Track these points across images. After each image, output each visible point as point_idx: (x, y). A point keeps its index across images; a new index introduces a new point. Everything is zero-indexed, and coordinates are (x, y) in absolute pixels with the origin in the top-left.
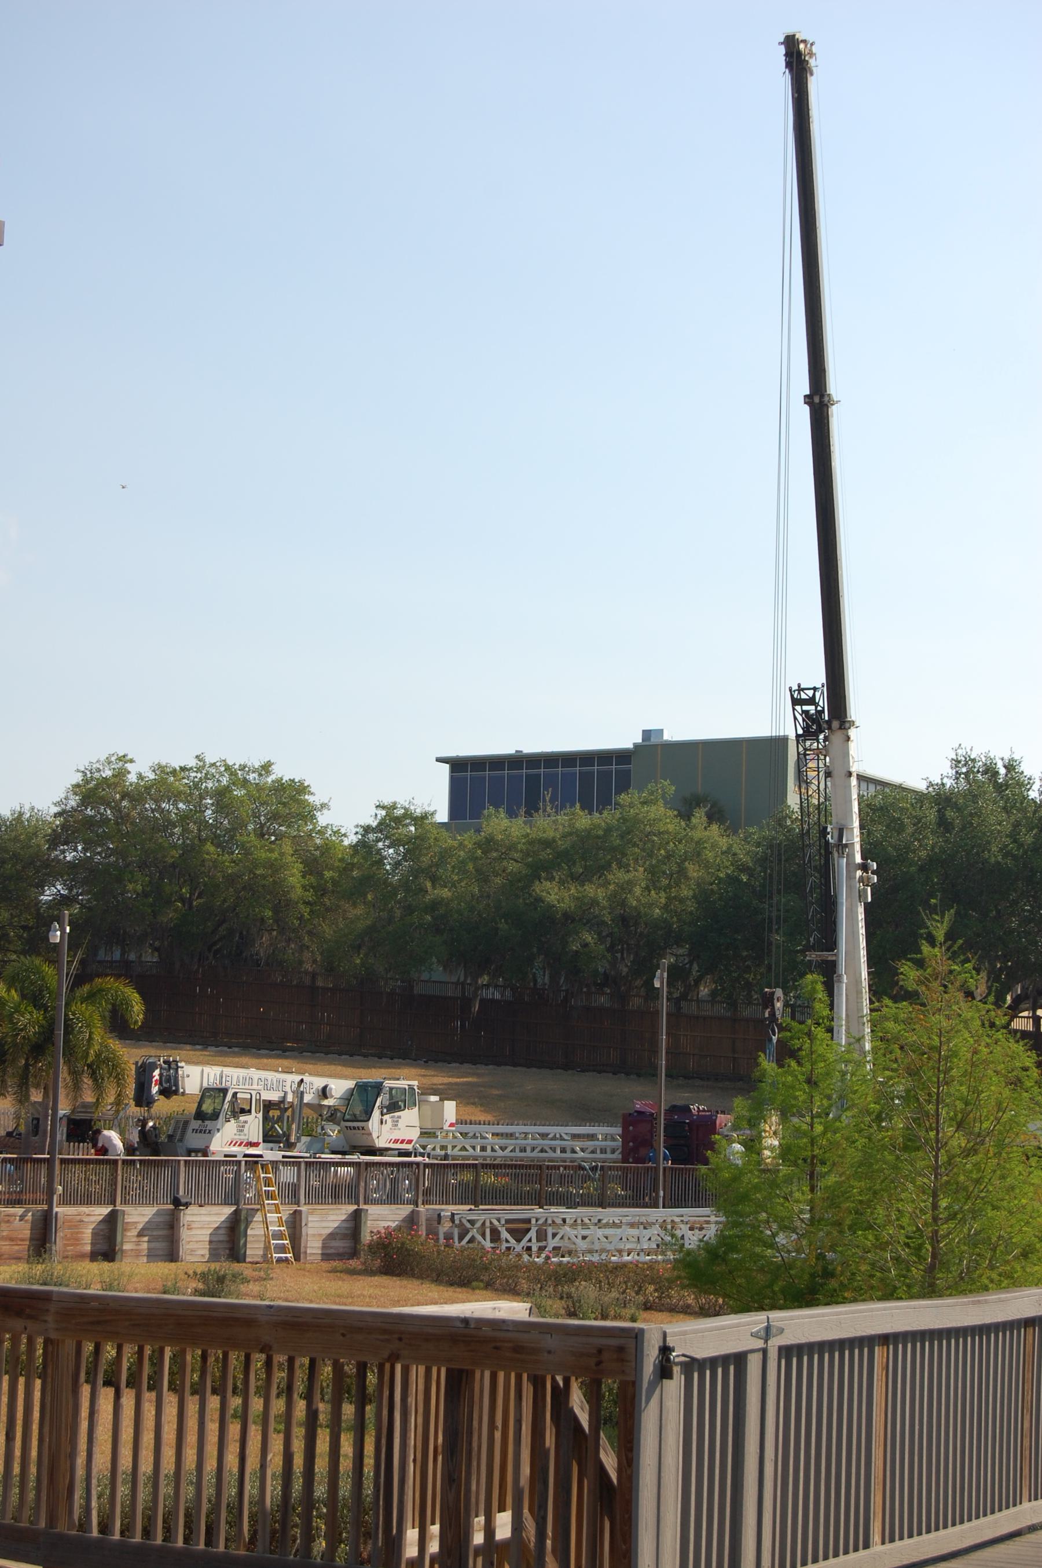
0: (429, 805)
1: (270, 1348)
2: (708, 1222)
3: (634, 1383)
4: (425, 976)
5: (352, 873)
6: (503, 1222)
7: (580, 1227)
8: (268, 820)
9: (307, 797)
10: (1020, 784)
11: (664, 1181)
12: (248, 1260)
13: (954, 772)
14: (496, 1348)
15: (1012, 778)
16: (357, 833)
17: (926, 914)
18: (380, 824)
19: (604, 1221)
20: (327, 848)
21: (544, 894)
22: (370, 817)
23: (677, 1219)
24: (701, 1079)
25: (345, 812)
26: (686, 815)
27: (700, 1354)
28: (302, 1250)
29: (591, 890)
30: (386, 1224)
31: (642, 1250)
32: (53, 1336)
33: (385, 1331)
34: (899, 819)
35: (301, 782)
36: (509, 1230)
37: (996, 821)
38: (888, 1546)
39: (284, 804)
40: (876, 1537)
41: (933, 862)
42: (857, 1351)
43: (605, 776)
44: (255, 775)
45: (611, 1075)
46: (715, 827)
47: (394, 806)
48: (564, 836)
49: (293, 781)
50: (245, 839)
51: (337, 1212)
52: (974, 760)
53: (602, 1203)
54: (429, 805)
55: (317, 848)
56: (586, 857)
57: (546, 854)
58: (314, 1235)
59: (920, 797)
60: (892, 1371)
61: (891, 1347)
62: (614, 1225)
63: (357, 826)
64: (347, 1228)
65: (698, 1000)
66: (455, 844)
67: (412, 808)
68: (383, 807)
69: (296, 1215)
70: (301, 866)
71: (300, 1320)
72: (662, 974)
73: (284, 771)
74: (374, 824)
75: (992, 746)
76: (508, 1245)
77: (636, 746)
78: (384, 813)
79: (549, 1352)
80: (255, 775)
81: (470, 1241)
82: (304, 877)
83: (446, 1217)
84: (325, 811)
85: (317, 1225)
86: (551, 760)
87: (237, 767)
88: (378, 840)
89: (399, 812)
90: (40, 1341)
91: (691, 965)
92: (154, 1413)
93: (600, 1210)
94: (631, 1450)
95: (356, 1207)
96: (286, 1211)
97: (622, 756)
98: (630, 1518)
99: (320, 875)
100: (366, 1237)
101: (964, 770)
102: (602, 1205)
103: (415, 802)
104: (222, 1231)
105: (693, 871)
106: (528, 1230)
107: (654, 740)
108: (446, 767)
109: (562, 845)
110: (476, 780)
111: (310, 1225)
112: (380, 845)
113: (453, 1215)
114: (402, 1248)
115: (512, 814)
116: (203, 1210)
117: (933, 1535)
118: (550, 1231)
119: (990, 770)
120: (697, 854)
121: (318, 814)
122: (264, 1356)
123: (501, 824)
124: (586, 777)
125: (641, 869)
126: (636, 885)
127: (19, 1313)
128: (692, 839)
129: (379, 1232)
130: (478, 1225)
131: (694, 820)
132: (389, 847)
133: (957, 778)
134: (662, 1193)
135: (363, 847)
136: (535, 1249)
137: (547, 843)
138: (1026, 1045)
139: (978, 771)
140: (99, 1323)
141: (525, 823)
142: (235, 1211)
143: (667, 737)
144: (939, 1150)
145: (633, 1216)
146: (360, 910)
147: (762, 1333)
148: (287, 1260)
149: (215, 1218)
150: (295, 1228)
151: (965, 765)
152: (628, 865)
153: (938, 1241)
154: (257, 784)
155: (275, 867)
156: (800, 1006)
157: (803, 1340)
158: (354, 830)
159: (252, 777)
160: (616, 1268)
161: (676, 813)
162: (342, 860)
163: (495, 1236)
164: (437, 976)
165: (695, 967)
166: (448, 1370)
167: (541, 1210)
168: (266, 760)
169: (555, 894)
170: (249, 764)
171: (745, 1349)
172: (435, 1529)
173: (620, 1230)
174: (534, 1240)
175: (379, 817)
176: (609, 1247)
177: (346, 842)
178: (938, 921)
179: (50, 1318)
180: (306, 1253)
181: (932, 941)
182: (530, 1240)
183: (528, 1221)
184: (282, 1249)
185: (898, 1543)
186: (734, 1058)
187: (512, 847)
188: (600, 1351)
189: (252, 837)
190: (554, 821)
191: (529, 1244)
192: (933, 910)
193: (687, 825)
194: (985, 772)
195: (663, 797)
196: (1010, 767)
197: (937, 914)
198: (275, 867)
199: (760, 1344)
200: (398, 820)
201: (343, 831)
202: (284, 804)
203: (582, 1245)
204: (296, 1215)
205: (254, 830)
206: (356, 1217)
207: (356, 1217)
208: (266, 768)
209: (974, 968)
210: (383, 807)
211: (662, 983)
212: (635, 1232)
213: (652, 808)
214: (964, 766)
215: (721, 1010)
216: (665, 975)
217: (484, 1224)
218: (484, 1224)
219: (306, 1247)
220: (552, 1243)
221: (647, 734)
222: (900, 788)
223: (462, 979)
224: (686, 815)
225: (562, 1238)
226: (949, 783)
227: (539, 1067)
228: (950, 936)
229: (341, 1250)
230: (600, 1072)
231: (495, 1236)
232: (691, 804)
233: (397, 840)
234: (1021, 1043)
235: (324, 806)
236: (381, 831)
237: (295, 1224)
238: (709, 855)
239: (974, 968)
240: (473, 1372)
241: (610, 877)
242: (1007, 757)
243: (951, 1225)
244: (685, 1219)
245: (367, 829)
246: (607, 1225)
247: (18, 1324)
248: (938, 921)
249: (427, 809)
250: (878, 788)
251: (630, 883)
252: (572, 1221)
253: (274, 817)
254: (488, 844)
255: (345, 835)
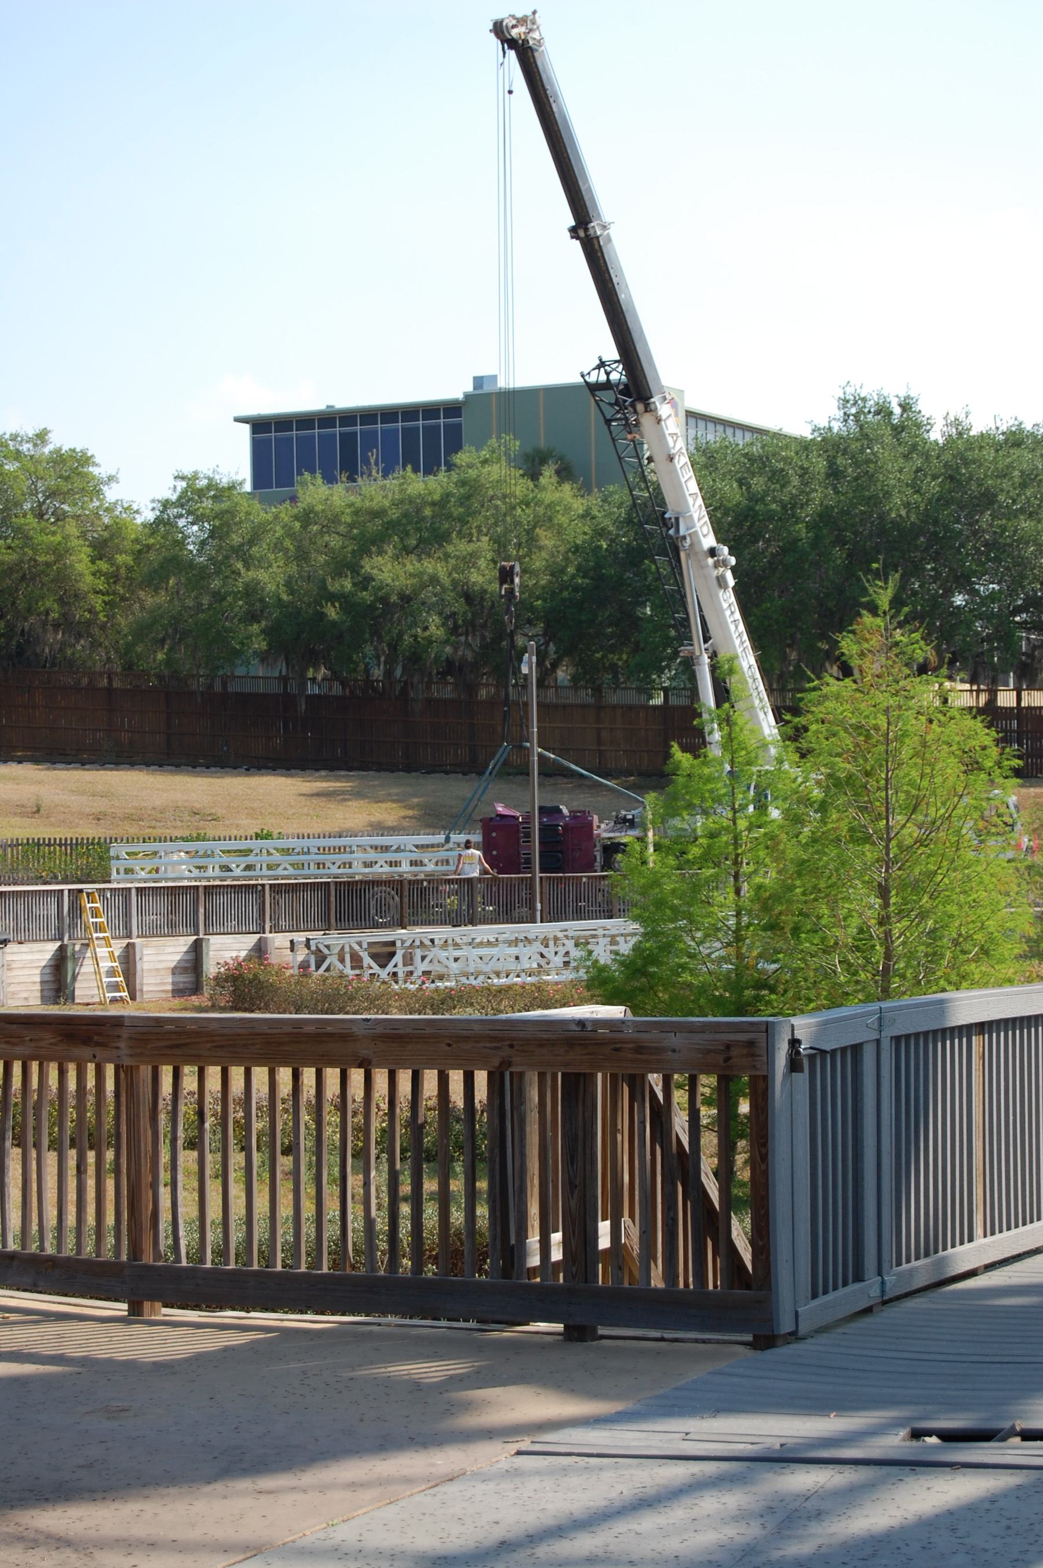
0: (237, 473)
1: (370, 1062)
2: (594, 936)
3: (765, 1078)
4: (240, 671)
5: (153, 556)
6: (365, 946)
7: (451, 948)
8: (47, 498)
9: (91, 469)
10: (919, 426)
11: (541, 893)
12: (77, 1001)
13: (842, 413)
14: (616, 1049)
15: (908, 419)
16: (153, 509)
17: (868, 581)
18: (180, 498)
19: (478, 940)
20: (116, 530)
21: (375, 571)
22: (168, 489)
23: (560, 935)
24: (564, 776)
25: (138, 484)
26: (534, 475)
27: (828, 1047)
28: (138, 987)
29: (431, 566)
30: (234, 954)
31: (523, 971)
32: (127, 1062)
33: (494, 1039)
34: (782, 470)
35: (83, 453)
36: (373, 956)
37: (894, 472)
38: (990, 1239)
39: (67, 479)
40: (979, 1230)
41: (825, 517)
42: (957, 1041)
43: (432, 432)
44: (30, 446)
45: (460, 776)
46: (567, 487)
47: (195, 477)
48: (395, 504)
49: (74, 450)
50: (22, 521)
51: (175, 943)
52: (864, 400)
53: (472, 921)
54: (237, 473)
55: (107, 527)
56: (422, 530)
57: (375, 527)
58: (150, 970)
59: (805, 446)
60: (988, 1060)
61: (986, 1036)
62: (489, 943)
63: (153, 501)
64: (186, 961)
65: (557, 687)
66: (269, 517)
67: (217, 477)
68: (183, 478)
69: (130, 949)
70: (89, 549)
71: (400, 1032)
72: (530, 658)
73: (62, 440)
74: (174, 497)
75: (884, 384)
76: (371, 971)
77: (467, 396)
78: (184, 484)
79: (674, 1051)
80: (30, 446)
81: (328, 970)
82: (93, 562)
83: (300, 943)
84: (113, 485)
85: (152, 958)
86: (369, 416)
87: (7, 436)
88: (181, 516)
89: (203, 483)
90: (110, 1070)
91: (547, 647)
92: (20, 1171)
93: (470, 927)
94: (765, 1145)
95: (195, 937)
96: (118, 946)
97: (452, 409)
98: (767, 1213)
99: (111, 560)
100: (211, 969)
101: (853, 411)
102: (472, 922)
103: (220, 470)
104: (47, 971)
105: (546, 539)
106: (392, 954)
107: (487, 388)
108: (246, 428)
109: (394, 514)
110: (285, 444)
111: (145, 959)
112: (181, 522)
113: (308, 940)
114: (254, 980)
115: (330, 479)
116: (24, 948)
117: (1029, 1227)
118: (418, 953)
119: (883, 411)
120: (547, 521)
121: (105, 488)
122: (362, 1071)
123: (317, 492)
124: (410, 435)
125: (485, 539)
126: (479, 558)
127: (87, 1041)
128: (542, 502)
129: (227, 964)
130: (336, 951)
131: (543, 481)
132: (193, 524)
133: (846, 421)
134: (539, 906)
135: (162, 524)
136: (401, 975)
137: (377, 514)
138: (982, 722)
139: (869, 412)
140: (177, 1046)
141: (347, 490)
142: (60, 946)
143: (502, 384)
144: (889, 840)
145: (512, 932)
146: (162, 598)
147: (876, 1026)
148: (122, 999)
149: (38, 956)
150: (128, 963)
151: (854, 404)
152: (471, 534)
153: (892, 942)
154: (32, 457)
155: (60, 552)
156: (675, 688)
157: (1018, 1015)
158: (151, 506)
159: (25, 447)
160: (500, 991)
161: (521, 472)
162: (136, 541)
163: (357, 962)
164: (256, 672)
165: (552, 647)
166: (563, 1074)
167: (404, 931)
168: (42, 427)
169: (388, 570)
170: (22, 433)
171: (861, 1041)
172: (557, 1237)
173: (497, 949)
174: (400, 965)
175: (179, 489)
176: (487, 969)
177: (139, 520)
178: (881, 587)
179: (122, 1044)
180: (142, 990)
181: (874, 610)
182: (395, 966)
183: (393, 943)
184: (116, 987)
185: (998, 1236)
186: (600, 751)
187: (335, 519)
188: (728, 1047)
189: (31, 519)
190: (381, 487)
191: (395, 970)
192: (877, 574)
193: (536, 486)
194: (878, 413)
195: (507, 454)
196: (905, 407)
197: (880, 580)
198: (60, 552)
199: (875, 1036)
200: (201, 493)
201: (135, 507)
202: (67, 479)
203: (455, 967)
204: (130, 949)
205: (32, 509)
206: (197, 948)
207: (197, 948)
208: (42, 437)
209: (922, 638)
210: (183, 478)
211: (531, 668)
212: (514, 951)
213: (488, 465)
214: (854, 406)
215: (585, 696)
216: (534, 659)
217: (343, 948)
218: (343, 948)
219: (142, 984)
220: (421, 967)
221: (478, 381)
222: (777, 436)
223: (284, 673)
224: (534, 475)
225: (431, 961)
226: (836, 426)
227: (378, 770)
228: (897, 602)
229: (181, 986)
230: (447, 773)
231: (357, 962)
232: (533, 461)
233: (202, 514)
234: (979, 718)
235: (111, 479)
236: (182, 506)
237: (128, 960)
238: (562, 519)
239: (922, 638)
240: (593, 1077)
241: (450, 549)
242: (902, 394)
243: (905, 923)
244: (570, 933)
245: (166, 504)
246: (481, 944)
247: (86, 1051)
248: (881, 587)
249: (234, 478)
250: (755, 435)
251: (474, 555)
252: (442, 942)
253: (52, 494)
254: (307, 517)
255: (137, 512)
